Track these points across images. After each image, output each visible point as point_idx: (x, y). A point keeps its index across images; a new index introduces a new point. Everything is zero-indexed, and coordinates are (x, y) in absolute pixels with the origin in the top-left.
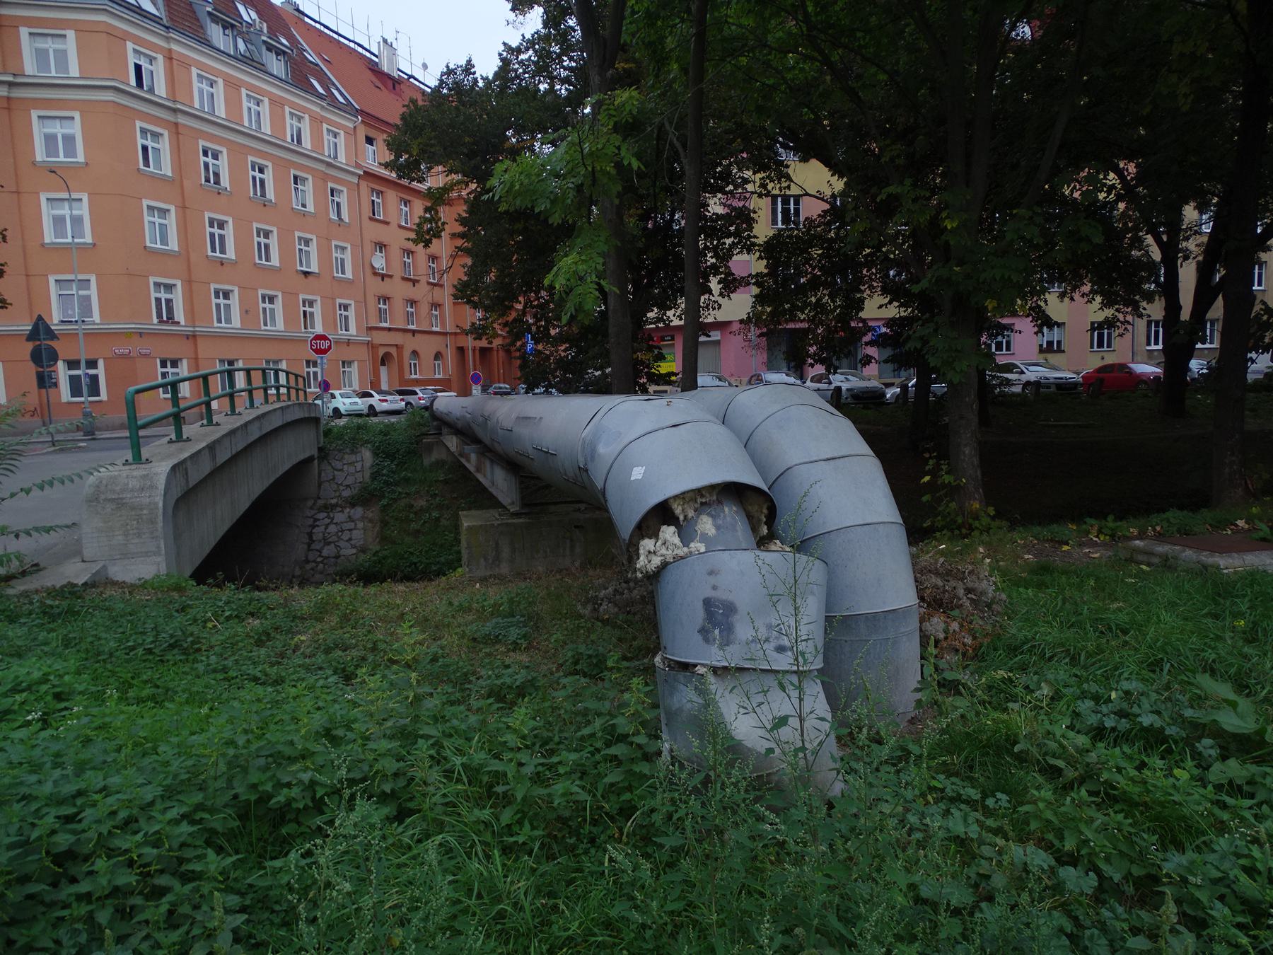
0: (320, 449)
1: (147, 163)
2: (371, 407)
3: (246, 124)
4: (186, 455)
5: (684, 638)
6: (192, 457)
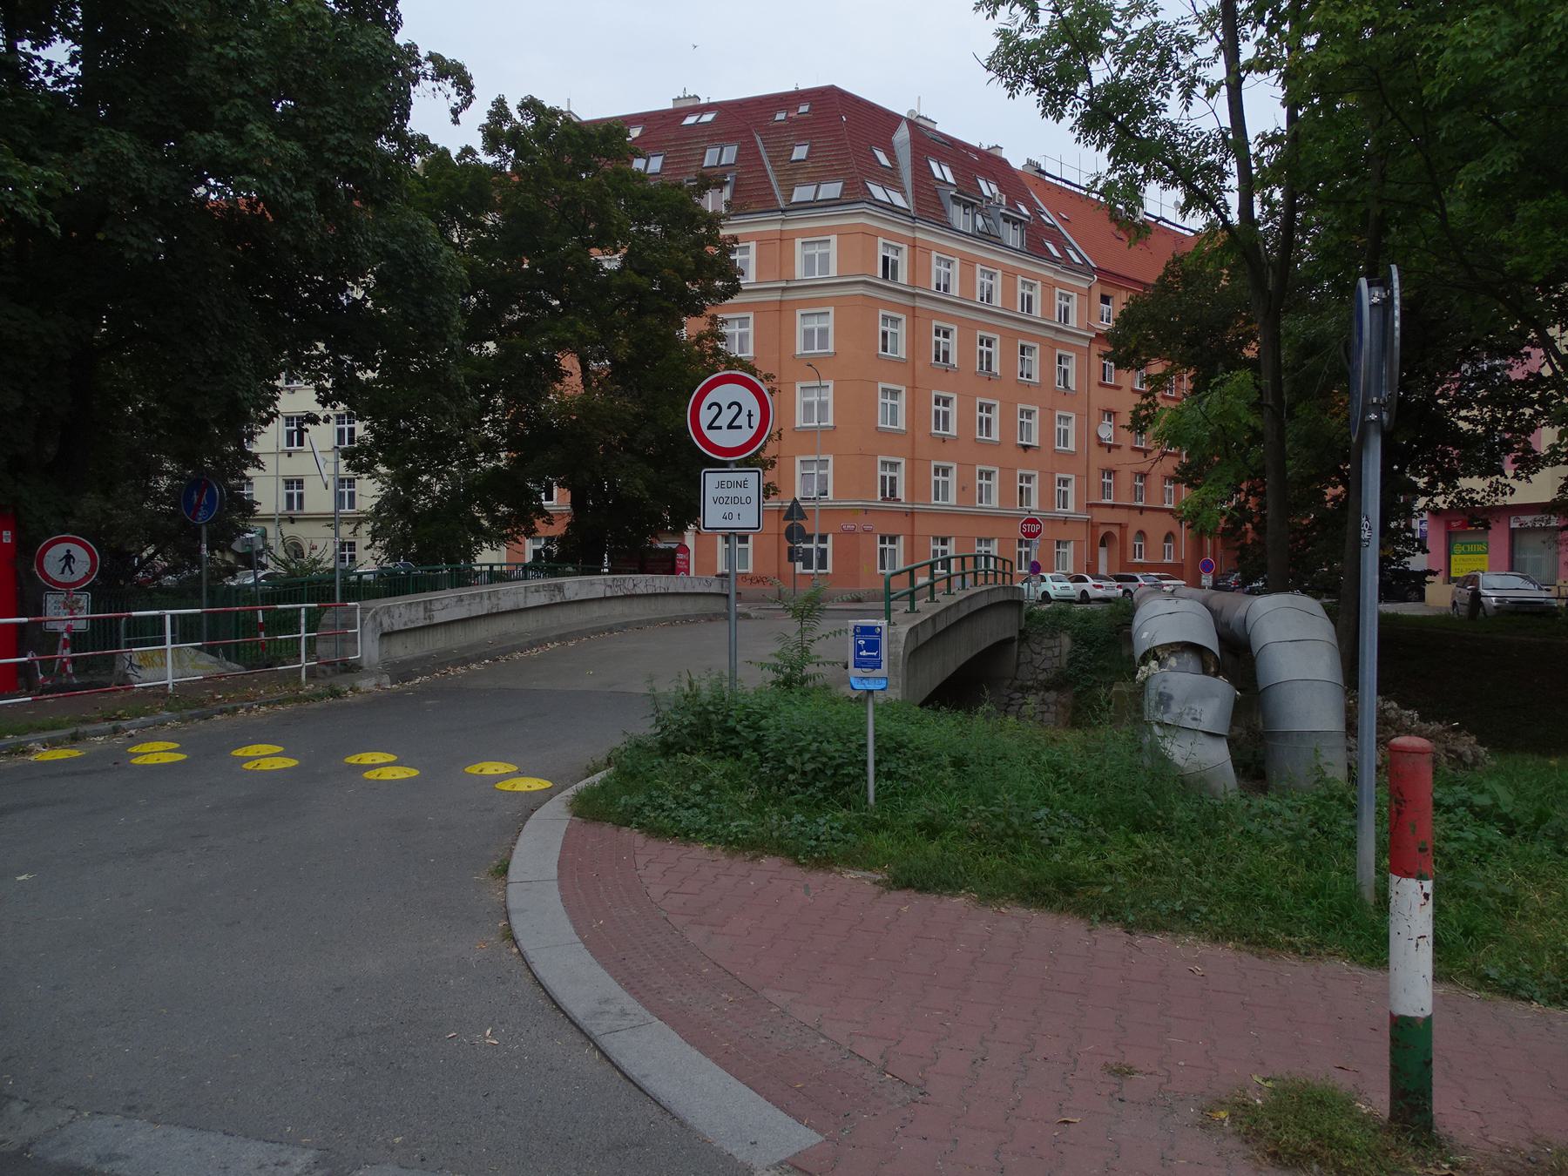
1: (885, 349)
2: (1084, 593)
5: (1152, 713)
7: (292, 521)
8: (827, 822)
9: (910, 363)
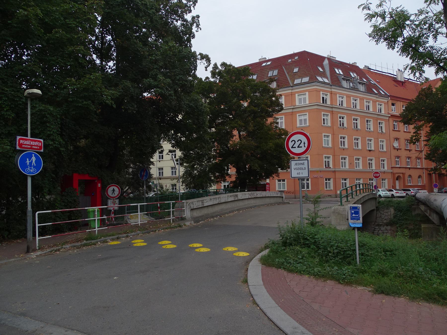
0: (377, 207)
1: (324, 123)
2: (392, 195)
7: (160, 179)
8: (347, 269)
9: (332, 127)
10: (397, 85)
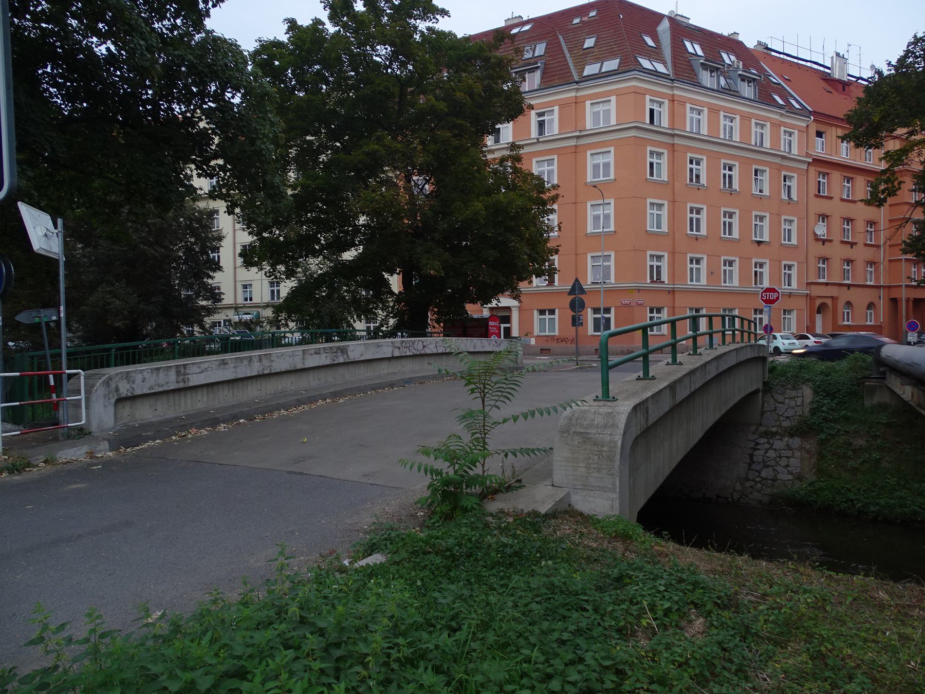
0: (765, 384)
1: (652, 174)
3: (722, 137)
4: (649, 394)
6: (652, 396)
10: (830, 89)
